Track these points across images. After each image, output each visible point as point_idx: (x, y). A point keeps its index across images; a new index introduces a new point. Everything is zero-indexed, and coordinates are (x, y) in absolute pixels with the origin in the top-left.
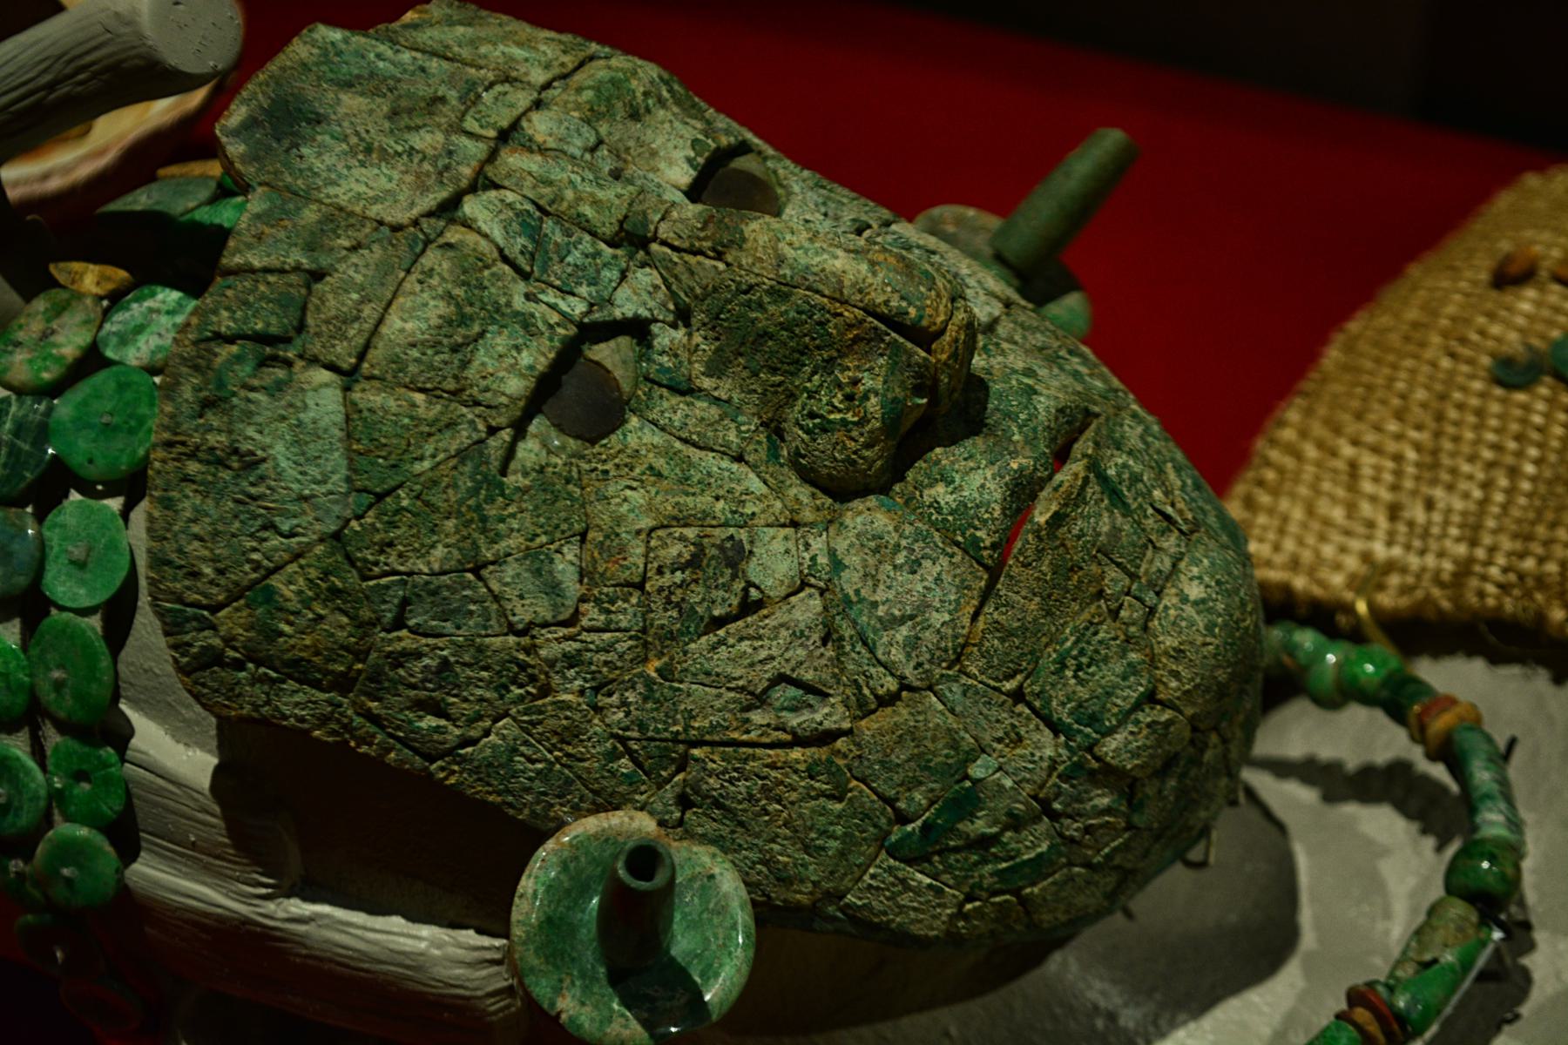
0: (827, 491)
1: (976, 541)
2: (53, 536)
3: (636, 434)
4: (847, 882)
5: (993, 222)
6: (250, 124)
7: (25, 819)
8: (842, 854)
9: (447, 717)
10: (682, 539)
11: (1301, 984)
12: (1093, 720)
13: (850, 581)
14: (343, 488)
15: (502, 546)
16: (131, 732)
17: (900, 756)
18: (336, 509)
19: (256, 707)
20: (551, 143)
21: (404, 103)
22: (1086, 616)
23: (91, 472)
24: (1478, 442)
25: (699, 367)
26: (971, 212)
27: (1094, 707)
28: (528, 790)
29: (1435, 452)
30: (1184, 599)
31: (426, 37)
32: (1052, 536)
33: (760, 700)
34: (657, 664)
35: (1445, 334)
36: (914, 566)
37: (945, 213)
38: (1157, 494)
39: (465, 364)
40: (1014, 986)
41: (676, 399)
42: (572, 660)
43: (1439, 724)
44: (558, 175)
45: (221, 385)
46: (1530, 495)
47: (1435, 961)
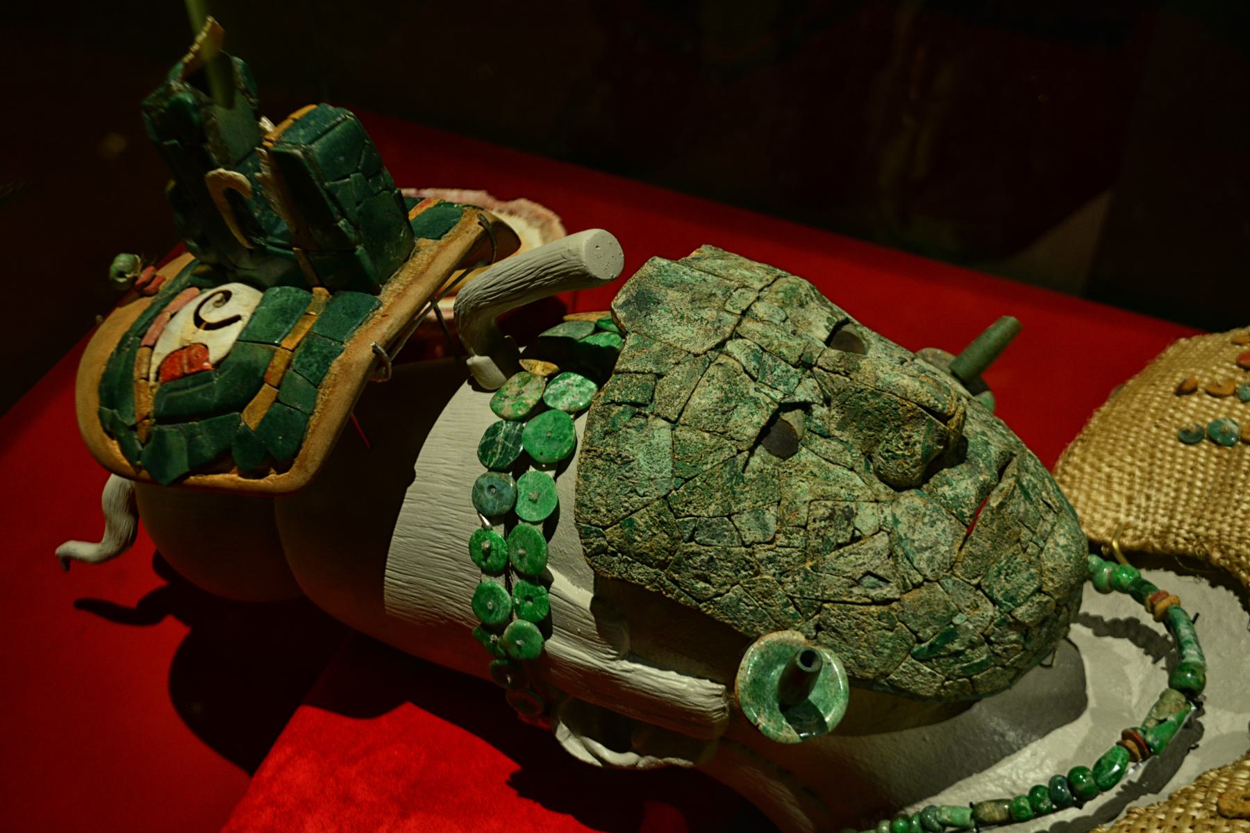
0: (891, 486)
1: (962, 514)
2: (522, 488)
3: (804, 456)
4: (891, 669)
5: (950, 357)
6: (627, 303)
7: (500, 617)
8: (890, 656)
9: (710, 583)
10: (825, 506)
11: (1091, 724)
12: (1012, 599)
13: (902, 529)
14: (670, 475)
15: (741, 506)
16: (552, 580)
17: (921, 612)
18: (666, 485)
19: (620, 574)
20: (766, 318)
21: (697, 296)
22: (1012, 550)
23: (540, 459)
24: (1172, 469)
25: (833, 426)
26: (939, 352)
27: (1013, 593)
28: (744, 619)
29: (1151, 473)
30: (1057, 545)
31: (703, 264)
32: (998, 513)
33: (858, 583)
34: (811, 563)
35: (1153, 416)
36: (933, 524)
37: (928, 351)
38: (1044, 494)
39: (727, 420)
40: (957, 718)
41: (822, 440)
42: (771, 560)
43: (1161, 605)
44: (770, 333)
45: (614, 425)
46: (1199, 497)
47: (1165, 720)
